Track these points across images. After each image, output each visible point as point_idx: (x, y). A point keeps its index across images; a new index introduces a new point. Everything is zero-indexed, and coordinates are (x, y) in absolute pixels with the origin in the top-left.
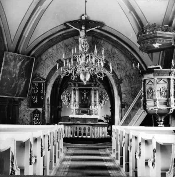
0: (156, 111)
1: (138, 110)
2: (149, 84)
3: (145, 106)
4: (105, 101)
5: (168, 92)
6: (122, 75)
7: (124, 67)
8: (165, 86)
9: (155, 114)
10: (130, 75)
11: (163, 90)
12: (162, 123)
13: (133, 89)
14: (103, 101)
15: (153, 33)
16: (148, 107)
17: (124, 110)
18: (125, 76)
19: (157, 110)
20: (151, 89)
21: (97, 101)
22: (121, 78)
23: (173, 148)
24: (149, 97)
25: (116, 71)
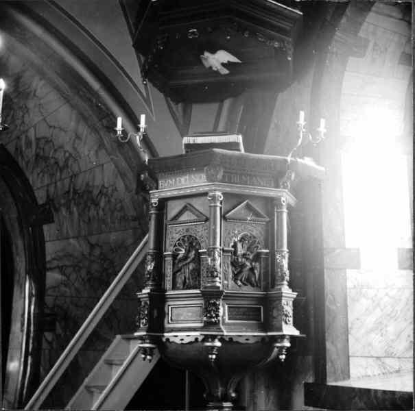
1: (112, 342)
2: (184, 217)
3: (157, 325)
6: (56, 187)
10: (91, 192)
13: (97, 252)
16: (172, 330)
17: (50, 343)
18: (68, 192)
19: (218, 344)
22: (50, 200)
24: (180, 281)
25: (31, 166)
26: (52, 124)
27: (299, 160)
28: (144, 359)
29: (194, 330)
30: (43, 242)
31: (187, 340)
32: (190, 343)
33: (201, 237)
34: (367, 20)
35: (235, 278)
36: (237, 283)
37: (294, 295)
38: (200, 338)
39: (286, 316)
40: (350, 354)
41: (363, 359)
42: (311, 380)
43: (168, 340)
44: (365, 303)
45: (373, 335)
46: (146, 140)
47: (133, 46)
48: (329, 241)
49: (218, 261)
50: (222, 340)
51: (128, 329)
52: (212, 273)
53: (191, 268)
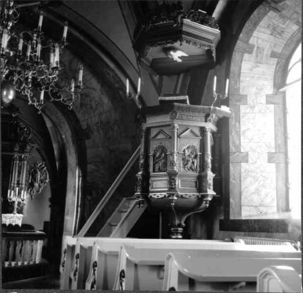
0: (174, 201)
2: (159, 137)
3: (146, 190)
4: (41, 185)
5: (200, 158)
7: (97, 103)
8: (195, 144)
9: (170, 207)
11: (189, 154)
12: (180, 229)
14: (36, 185)
15: (176, 21)
16: (153, 192)
18: (98, 123)
19: (175, 198)
20: (163, 149)
21: (24, 182)
22: (89, 127)
23: (87, 226)
24: (157, 168)
26: (89, 86)
27: (217, 108)
28: (139, 207)
29: (164, 191)
30: (85, 149)
31: (160, 197)
32: (162, 198)
33: (167, 146)
34: (254, 35)
35: (185, 165)
36: (185, 169)
37: (214, 175)
38: (167, 196)
39: (209, 185)
40: (242, 204)
41: (249, 207)
42: (222, 218)
43: (151, 197)
44: (249, 180)
45: (254, 195)
46: (140, 97)
47: (134, 47)
48: (232, 148)
49: (176, 158)
50: (177, 196)
51: (130, 194)
52: (173, 164)
53: (162, 161)
